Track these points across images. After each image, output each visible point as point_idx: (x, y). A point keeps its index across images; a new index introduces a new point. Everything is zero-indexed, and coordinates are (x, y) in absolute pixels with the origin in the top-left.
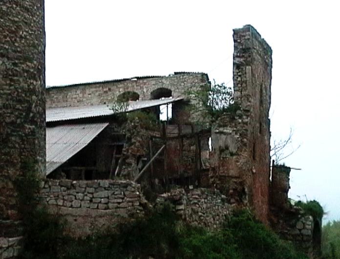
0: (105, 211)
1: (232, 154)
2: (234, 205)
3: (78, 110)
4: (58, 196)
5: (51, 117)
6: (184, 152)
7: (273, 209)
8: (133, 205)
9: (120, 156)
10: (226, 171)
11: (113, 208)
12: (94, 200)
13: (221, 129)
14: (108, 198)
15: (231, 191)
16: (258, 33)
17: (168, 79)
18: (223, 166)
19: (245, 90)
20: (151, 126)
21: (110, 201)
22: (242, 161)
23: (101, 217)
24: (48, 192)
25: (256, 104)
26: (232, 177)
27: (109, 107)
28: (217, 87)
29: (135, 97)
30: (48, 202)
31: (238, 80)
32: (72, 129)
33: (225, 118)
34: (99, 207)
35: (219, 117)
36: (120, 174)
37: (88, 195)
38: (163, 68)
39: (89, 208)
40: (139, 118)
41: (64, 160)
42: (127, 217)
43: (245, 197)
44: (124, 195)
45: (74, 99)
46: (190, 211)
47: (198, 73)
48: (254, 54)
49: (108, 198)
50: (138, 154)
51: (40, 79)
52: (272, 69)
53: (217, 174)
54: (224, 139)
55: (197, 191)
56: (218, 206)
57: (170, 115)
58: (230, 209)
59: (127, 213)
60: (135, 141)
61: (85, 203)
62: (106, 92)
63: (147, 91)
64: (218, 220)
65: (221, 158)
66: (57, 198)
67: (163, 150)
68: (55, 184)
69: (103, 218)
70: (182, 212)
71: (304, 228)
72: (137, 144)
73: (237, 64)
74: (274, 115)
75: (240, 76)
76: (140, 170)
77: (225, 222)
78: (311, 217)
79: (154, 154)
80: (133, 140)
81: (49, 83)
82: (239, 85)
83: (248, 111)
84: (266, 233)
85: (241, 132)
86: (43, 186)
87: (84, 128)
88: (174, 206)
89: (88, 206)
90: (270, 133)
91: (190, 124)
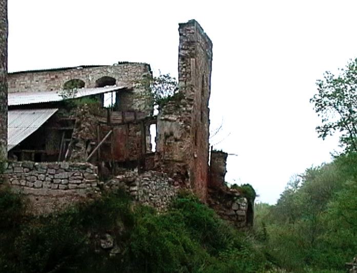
0: (65, 191)
1: (176, 140)
2: (178, 187)
3: (28, 96)
4: (21, 177)
5: (13, 100)
6: (130, 137)
7: (210, 191)
8: (91, 186)
9: (69, 140)
10: (170, 156)
11: (72, 189)
12: (54, 181)
13: (167, 117)
14: (68, 179)
15: (175, 174)
16: (201, 27)
17: (113, 68)
18: (168, 151)
19: (190, 80)
20: (99, 112)
21: (70, 182)
22: (185, 146)
23: (61, 196)
24: (11, 173)
25: (198, 93)
26: (176, 161)
27: (59, 94)
28: (163, 77)
29: (82, 85)
30: (11, 182)
31: (183, 71)
32: (14, 113)
33: (170, 106)
34: (60, 188)
35: (165, 105)
36: (70, 156)
37: (50, 176)
38: (107, 57)
39: (50, 188)
40: (88, 105)
41: (17, 143)
42: (85, 197)
43: (188, 180)
44: (84, 177)
45: (21, 86)
46: (142, 192)
47: (141, 63)
48: (198, 47)
49: (68, 179)
50: (87, 138)
51: (3, 66)
52: (213, 62)
53: (162, 158)
54: (169, 126)
55: (62, 193)
56: (166, 188)
57: (114, 102)
58: (175, 191)
59: (86, 193)
60: (84, 126)
61: (46, 184)
62: (53, 79)
63: (93, 79)
64: (165, 201)
65: (167, 144)
66: (20, 178)
67: (110, 135)
68: (18, 165)
69: (63, 198)
70: (136, 192)
71: (239, 209)
72: (86, 129)
73: (181, 56)
74: (213, 104)
75: (185, 67)
76: (89, 154)
77: (171, 203)
78: (245, 199)
79: (101, 139)
80: (82, 126)
81: (11, 70)
82: (184, 76)
83: (192, 100)
84: (208, 213)
85: (184, 119)
86: (7, 167)
87: (34, 113)
88: (128, 187)
89: (49, 186)
90: (209, 120)
91: (133, 111)
